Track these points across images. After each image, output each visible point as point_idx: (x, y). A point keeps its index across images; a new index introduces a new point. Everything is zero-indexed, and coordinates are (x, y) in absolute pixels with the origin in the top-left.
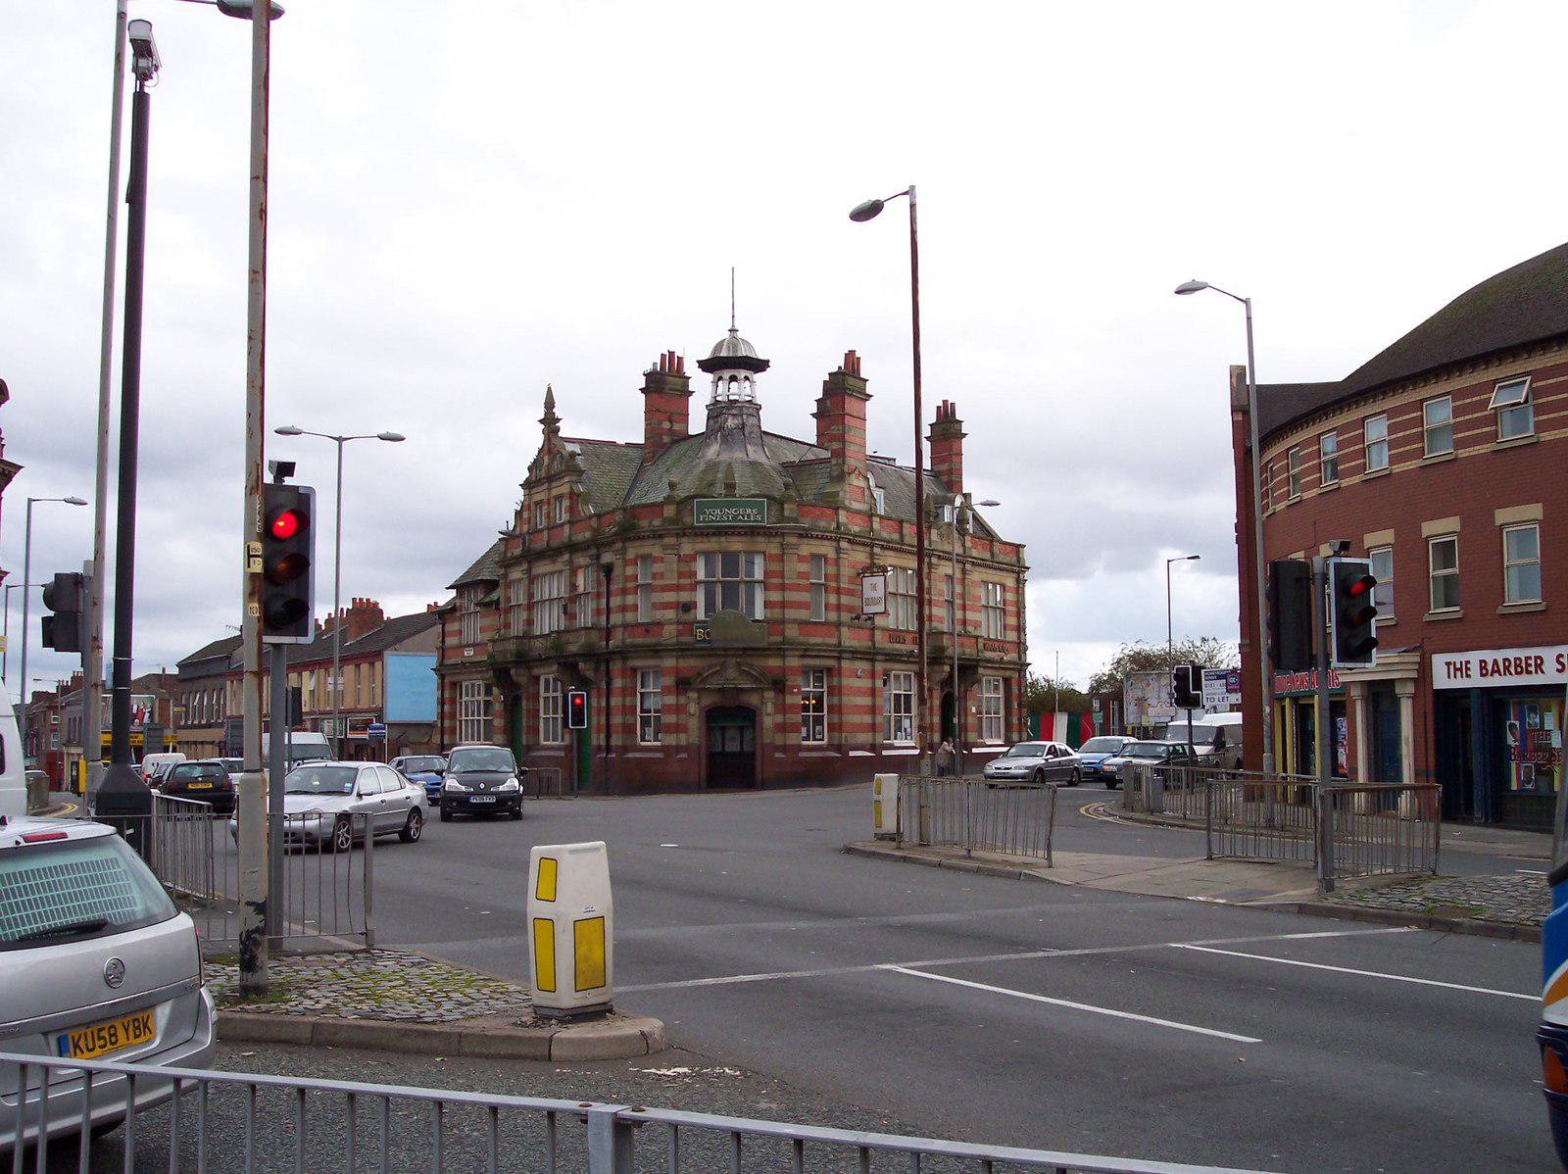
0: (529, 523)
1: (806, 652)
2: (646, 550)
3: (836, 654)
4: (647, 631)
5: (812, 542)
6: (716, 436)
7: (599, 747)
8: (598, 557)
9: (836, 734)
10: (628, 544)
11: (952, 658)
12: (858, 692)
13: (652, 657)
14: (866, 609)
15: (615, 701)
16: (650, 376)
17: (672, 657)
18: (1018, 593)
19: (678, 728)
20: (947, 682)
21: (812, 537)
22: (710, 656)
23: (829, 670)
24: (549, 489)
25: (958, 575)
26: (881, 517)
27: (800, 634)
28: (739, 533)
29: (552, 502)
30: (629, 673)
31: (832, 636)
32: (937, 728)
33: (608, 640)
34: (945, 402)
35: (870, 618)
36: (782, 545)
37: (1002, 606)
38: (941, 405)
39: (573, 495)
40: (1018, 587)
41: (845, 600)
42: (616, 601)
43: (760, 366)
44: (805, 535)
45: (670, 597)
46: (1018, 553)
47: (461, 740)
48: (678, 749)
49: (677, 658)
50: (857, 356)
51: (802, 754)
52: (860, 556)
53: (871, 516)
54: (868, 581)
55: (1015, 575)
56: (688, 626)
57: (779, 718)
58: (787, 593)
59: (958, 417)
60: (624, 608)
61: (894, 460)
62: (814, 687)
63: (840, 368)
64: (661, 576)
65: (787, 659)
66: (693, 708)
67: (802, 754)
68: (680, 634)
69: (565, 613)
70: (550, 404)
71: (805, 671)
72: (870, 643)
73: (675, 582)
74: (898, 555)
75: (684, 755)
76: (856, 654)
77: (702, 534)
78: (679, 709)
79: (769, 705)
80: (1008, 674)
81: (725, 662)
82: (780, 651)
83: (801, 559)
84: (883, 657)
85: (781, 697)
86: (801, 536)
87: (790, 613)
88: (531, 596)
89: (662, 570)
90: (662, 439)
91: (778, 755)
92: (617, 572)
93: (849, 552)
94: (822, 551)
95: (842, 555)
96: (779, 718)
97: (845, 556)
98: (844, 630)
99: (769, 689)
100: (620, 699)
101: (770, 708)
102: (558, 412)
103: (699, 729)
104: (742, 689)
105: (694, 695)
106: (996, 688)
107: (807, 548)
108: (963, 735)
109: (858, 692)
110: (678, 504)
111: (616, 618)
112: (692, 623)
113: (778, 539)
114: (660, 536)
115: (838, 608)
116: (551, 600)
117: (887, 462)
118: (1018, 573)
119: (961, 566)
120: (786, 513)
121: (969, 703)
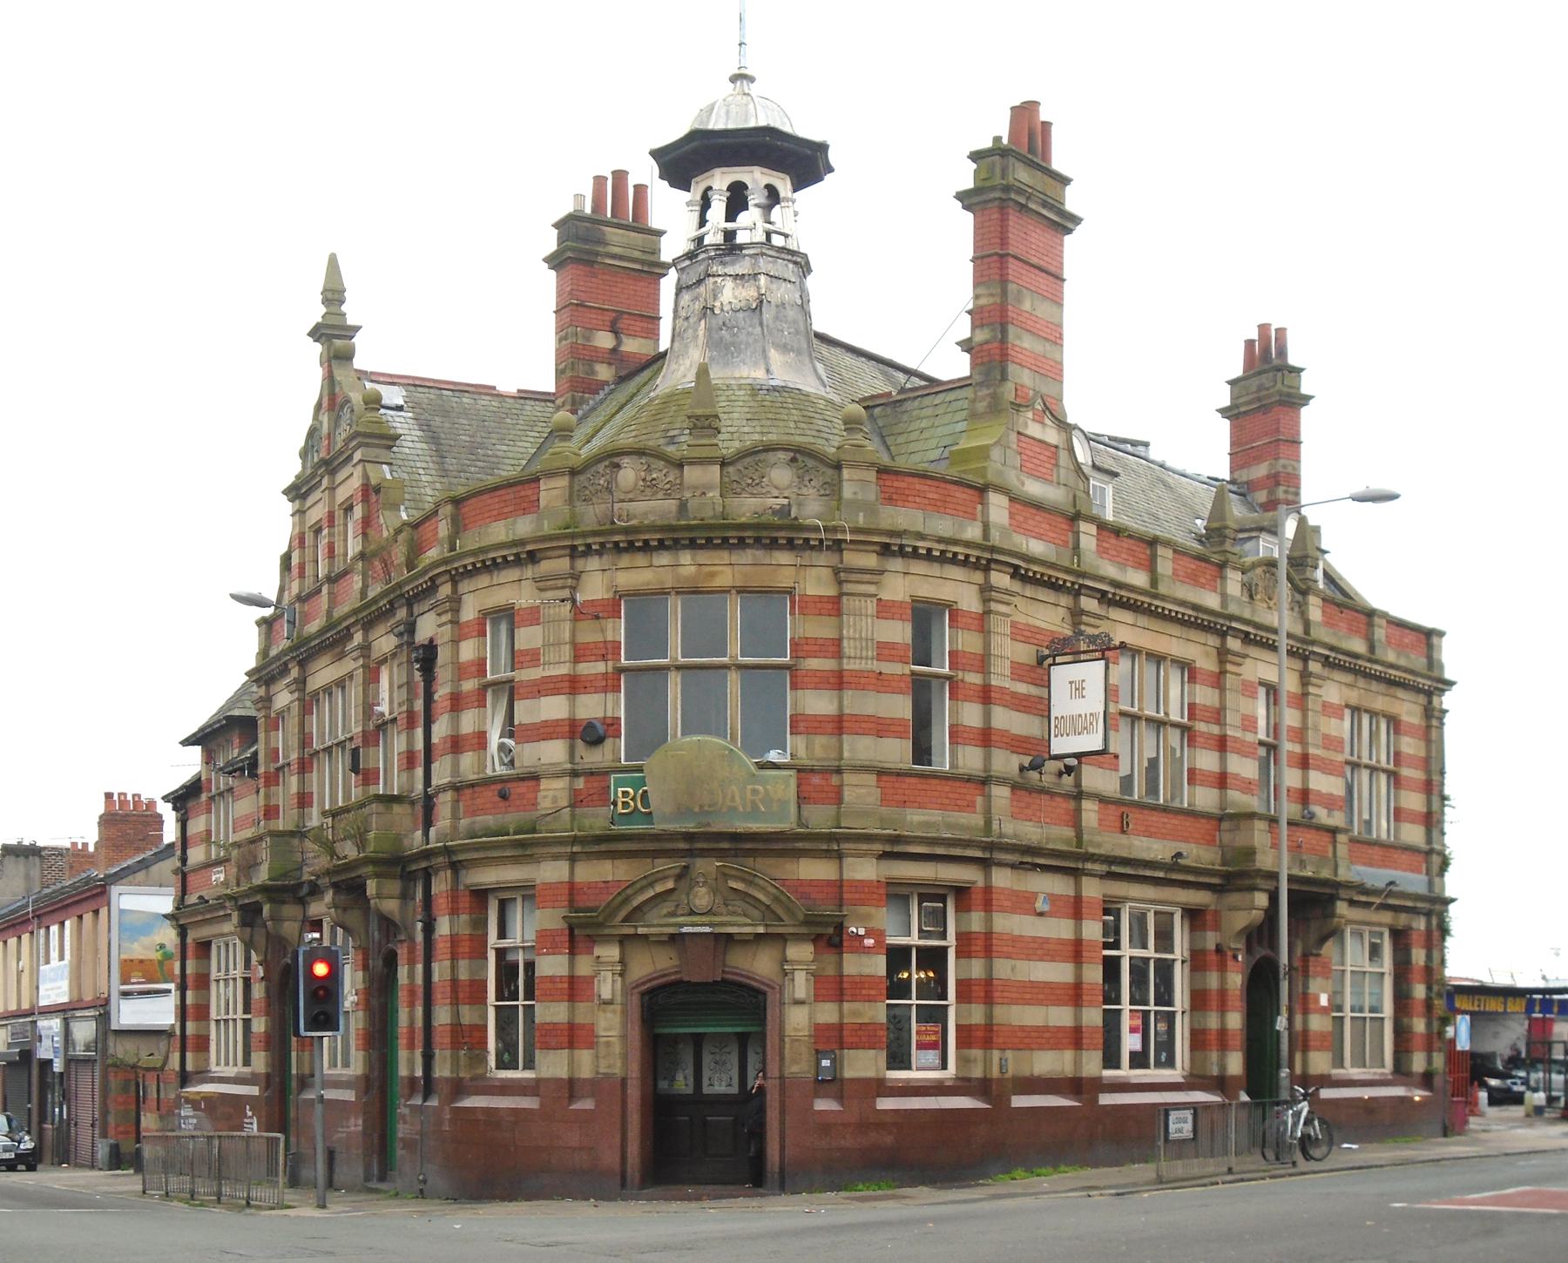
0: (302, 575)
1: (894, 848)
2: (499, 598)
3: (979, 854)
4: (504, 796)
5: (919, 567)
6: (696, 330)
7: (412, 1081)
8: (411, 628)
9: (977, 1053)
10: (464, 586)
11: (1274, 876)
12: (1041, 949)
13: (516, 860)
14: (1059, 746)
15: (440, 971)
16: (570, 227)
17: (556, 857)
18: (1428, 741)
19: (574, 1036)
20: (1263, 933)
21: (915, 554)
22: (656, 854)
23: (961, 893)
24: (332, 489)
25: (1290, 684)
26: (1102, 526)
27: (884, 801)
28: (709, 540)
29: (339, 520)
30: (465, 902)
31: (971, 806)
32: (1237, 1040)
33: (428, 823)
34: (1264, 329)
35: (1069, 770)
36: (836, 571)
37: (1391, 766)
38: (1255, 336)
39: (370, 491)
40: (1429, 727)
41: (1005, 719)
42: (440, 730)
43: (751, 79)
44: (892, 548)
45: (554, 708)
46: (1430, 647)
48: (572, 1087)
49: (573, 858)
50: (1043, 117)
51: (886, 1104)
52: (1049, 616)
53: (1075, 518)
54: (1062, 675)
55: (1422, 699)
56: (1302, 1041)
57: (828, 1013)
58: (848, 694)
59: (1293, 360)
60: (456, 744)
61: (1146, 445)
62: (923, 934)
63: (997, 139)
64: (533, 657)
65: (848, 861)
66: (607, 987)
67: (886, 1104)
68: (576, 801)
69: (355, 768)
70: (333, 295)
71: (897, 894)
72: (1069, 833)
73: (564, 670)
74: (1143, 621)
75: (587, 1104)
76: (1030, 858)
77: (631, 548)
78: (575, 988)
79: (800, 978)
80: (1403, 920)
81: (686, 868)
82: (831, 845)
83: (886, 610)
84: (1104, 868)
85: (830, 958)
86: (885, 550)
87: (860, 748)
88: (305, 741)
89: (538, 643)
90: (593, 372)
91: (822, 1105)
92: (443, 655)
93: (1016, 600)
94: (945, 592)
95: (994, 606)
96: (828, 1013)
97: (1002, 608)
98: (1001, 793)
99: (798, 938)
100: (1085, 1022)
101: (801, 985)
102: (353, 313)
103: (624, 1037)
104: (730, 935)
105: (611, 952)
106: (1375, 951)
107: (901, 584)
108: (1298, 1057)
109: (1041, 949)
110: (574, 473)
111: (442, 773)
112: (605, 773)
113: (824, 558)
114: (533, 557)
115: (986, 737)
116: (328, 750)
117: (1122, 446)
118: (1429, 694)
119: (1298, 665)
120: (848, 492)
121: (1315, 985)
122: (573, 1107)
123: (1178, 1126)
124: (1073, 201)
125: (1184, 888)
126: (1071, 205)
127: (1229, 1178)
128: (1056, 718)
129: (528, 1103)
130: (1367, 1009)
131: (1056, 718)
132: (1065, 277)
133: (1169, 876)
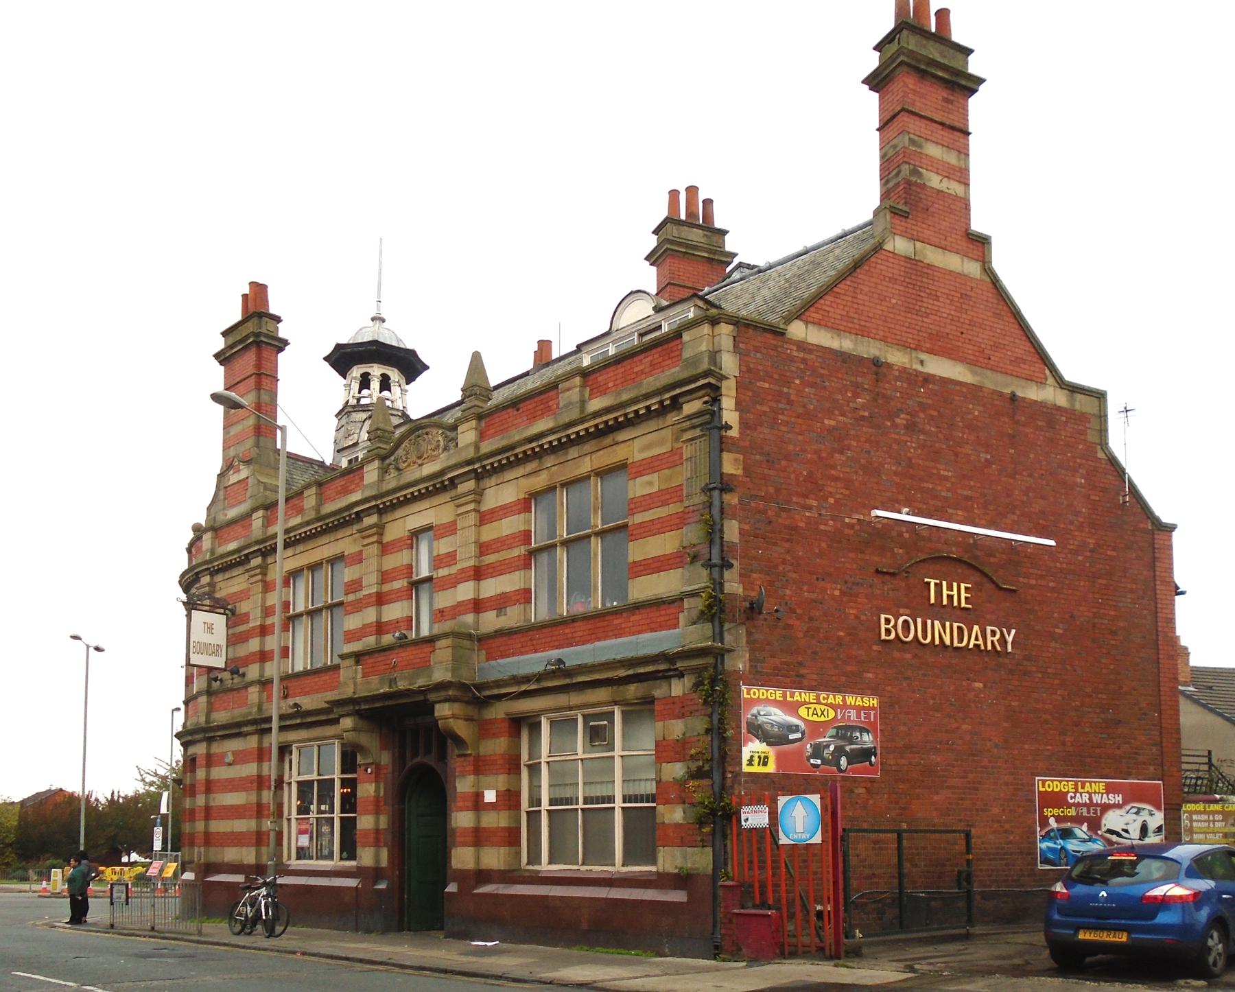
47: (534, 857)
122: (376, 887)
123: (119, 895)
124: (975, 66)
125: (331, 725)
126: (282, 334)
127: (151, 933)
128: (194, 642)
129: (352, 883)
130: (581, 800)
131: (194, 642)
132: (970, 130)
133: (304, 721)
